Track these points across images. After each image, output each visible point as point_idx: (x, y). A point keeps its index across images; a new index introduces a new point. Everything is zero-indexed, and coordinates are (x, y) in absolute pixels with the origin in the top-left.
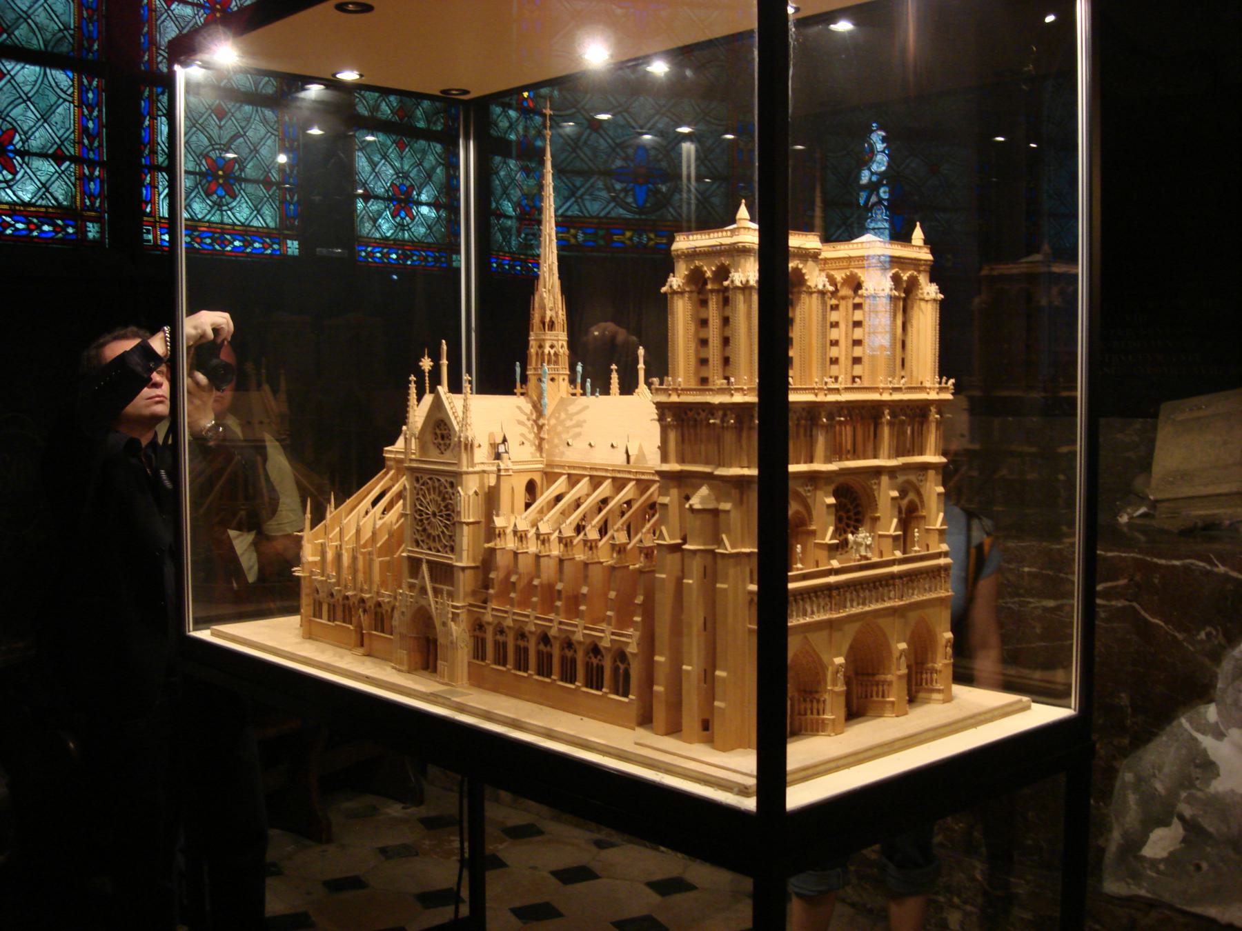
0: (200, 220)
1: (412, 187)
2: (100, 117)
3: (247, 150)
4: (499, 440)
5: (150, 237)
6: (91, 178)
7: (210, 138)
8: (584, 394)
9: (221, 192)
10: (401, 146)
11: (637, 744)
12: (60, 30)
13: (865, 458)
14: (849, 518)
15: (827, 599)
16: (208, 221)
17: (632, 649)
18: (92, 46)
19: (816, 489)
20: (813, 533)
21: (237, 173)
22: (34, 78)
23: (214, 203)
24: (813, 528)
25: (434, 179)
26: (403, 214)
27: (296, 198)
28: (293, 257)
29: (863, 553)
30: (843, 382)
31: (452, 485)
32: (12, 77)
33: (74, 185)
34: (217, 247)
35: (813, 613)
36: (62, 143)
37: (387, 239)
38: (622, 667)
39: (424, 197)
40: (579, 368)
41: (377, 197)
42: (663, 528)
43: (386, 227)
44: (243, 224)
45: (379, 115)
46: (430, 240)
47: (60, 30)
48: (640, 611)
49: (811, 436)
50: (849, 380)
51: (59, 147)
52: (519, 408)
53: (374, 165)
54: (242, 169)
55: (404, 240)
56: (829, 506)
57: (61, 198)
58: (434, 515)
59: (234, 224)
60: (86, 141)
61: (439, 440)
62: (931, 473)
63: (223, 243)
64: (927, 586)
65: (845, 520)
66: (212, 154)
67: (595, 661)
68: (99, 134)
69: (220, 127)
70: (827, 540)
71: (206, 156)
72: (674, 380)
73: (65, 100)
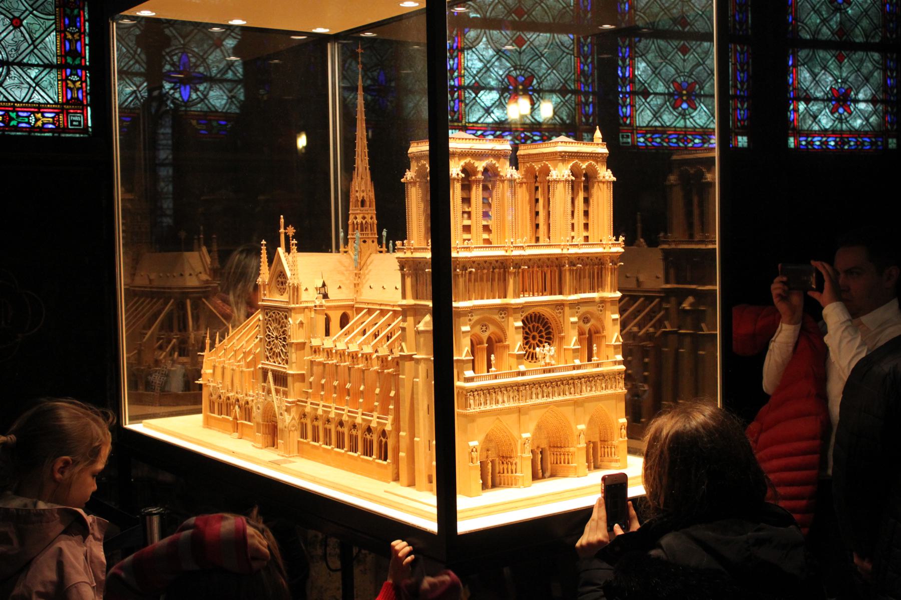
0: (668, 127)
1: (850, 89)
2: (592, 62)
3: (706, 74)
4: (320, 285)
5: (629, 140)
6: (587, 103)
7: (676, 69)
8: (388, 251)
9: (685, 106)
10: (840, 60)
11: (386, 492)
12: (564, 8)
13: (585, 292)
14: (541, 337)
15: (516, 393)
16: (675, 127)
17: (388, 428)
18: (586, 15)
19: (508, 316)
20: (508, 347)
21: (698, 92)
22: (546, 42)
23: (680, 114)
24: (507, 343)
25: (871, 80)
26: (841, 110)
27: (745, 106)
28: (743, 149)
29: (548, 361)
30: (579, 240)
31: (286, 317)
32: (531, 43)
33: (575, 109)
34: (681, 144)
35: (504, 402)
36: (566, 82)
37: (826, 130)
38: (384, 440)
39: (861, 96)
40: (384, 233)
41: (817, 99)
42: (403, 344)
43: (826, 121)
44: (702, 127)
45: (820, 37)
46: (867, 129)
47: (564, 8)
48: (392, 402)
49: (505, 280)
50: (534, 239)
51: (564, 85)
52: (340, 262)
53: (814, 75)
54: (701, 88)
55: (842, 130)
56: (517, 328)
57: (565, 118)
58: (277, 338)
59: (695, 127)
60: (583, 79)
61: (280, 286)
62: (608, 305)
63: (687, 141)
64: (603, 385)
65: (538, 338)
66: (678, 80)
67: (368, 437)
68: (592, 74)
69: (684, 61)
70: (516, 352)
71: (674, 82)
72: (409, 243)
73: (568, 54)
